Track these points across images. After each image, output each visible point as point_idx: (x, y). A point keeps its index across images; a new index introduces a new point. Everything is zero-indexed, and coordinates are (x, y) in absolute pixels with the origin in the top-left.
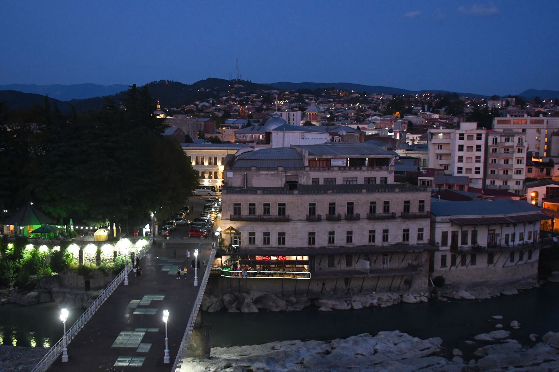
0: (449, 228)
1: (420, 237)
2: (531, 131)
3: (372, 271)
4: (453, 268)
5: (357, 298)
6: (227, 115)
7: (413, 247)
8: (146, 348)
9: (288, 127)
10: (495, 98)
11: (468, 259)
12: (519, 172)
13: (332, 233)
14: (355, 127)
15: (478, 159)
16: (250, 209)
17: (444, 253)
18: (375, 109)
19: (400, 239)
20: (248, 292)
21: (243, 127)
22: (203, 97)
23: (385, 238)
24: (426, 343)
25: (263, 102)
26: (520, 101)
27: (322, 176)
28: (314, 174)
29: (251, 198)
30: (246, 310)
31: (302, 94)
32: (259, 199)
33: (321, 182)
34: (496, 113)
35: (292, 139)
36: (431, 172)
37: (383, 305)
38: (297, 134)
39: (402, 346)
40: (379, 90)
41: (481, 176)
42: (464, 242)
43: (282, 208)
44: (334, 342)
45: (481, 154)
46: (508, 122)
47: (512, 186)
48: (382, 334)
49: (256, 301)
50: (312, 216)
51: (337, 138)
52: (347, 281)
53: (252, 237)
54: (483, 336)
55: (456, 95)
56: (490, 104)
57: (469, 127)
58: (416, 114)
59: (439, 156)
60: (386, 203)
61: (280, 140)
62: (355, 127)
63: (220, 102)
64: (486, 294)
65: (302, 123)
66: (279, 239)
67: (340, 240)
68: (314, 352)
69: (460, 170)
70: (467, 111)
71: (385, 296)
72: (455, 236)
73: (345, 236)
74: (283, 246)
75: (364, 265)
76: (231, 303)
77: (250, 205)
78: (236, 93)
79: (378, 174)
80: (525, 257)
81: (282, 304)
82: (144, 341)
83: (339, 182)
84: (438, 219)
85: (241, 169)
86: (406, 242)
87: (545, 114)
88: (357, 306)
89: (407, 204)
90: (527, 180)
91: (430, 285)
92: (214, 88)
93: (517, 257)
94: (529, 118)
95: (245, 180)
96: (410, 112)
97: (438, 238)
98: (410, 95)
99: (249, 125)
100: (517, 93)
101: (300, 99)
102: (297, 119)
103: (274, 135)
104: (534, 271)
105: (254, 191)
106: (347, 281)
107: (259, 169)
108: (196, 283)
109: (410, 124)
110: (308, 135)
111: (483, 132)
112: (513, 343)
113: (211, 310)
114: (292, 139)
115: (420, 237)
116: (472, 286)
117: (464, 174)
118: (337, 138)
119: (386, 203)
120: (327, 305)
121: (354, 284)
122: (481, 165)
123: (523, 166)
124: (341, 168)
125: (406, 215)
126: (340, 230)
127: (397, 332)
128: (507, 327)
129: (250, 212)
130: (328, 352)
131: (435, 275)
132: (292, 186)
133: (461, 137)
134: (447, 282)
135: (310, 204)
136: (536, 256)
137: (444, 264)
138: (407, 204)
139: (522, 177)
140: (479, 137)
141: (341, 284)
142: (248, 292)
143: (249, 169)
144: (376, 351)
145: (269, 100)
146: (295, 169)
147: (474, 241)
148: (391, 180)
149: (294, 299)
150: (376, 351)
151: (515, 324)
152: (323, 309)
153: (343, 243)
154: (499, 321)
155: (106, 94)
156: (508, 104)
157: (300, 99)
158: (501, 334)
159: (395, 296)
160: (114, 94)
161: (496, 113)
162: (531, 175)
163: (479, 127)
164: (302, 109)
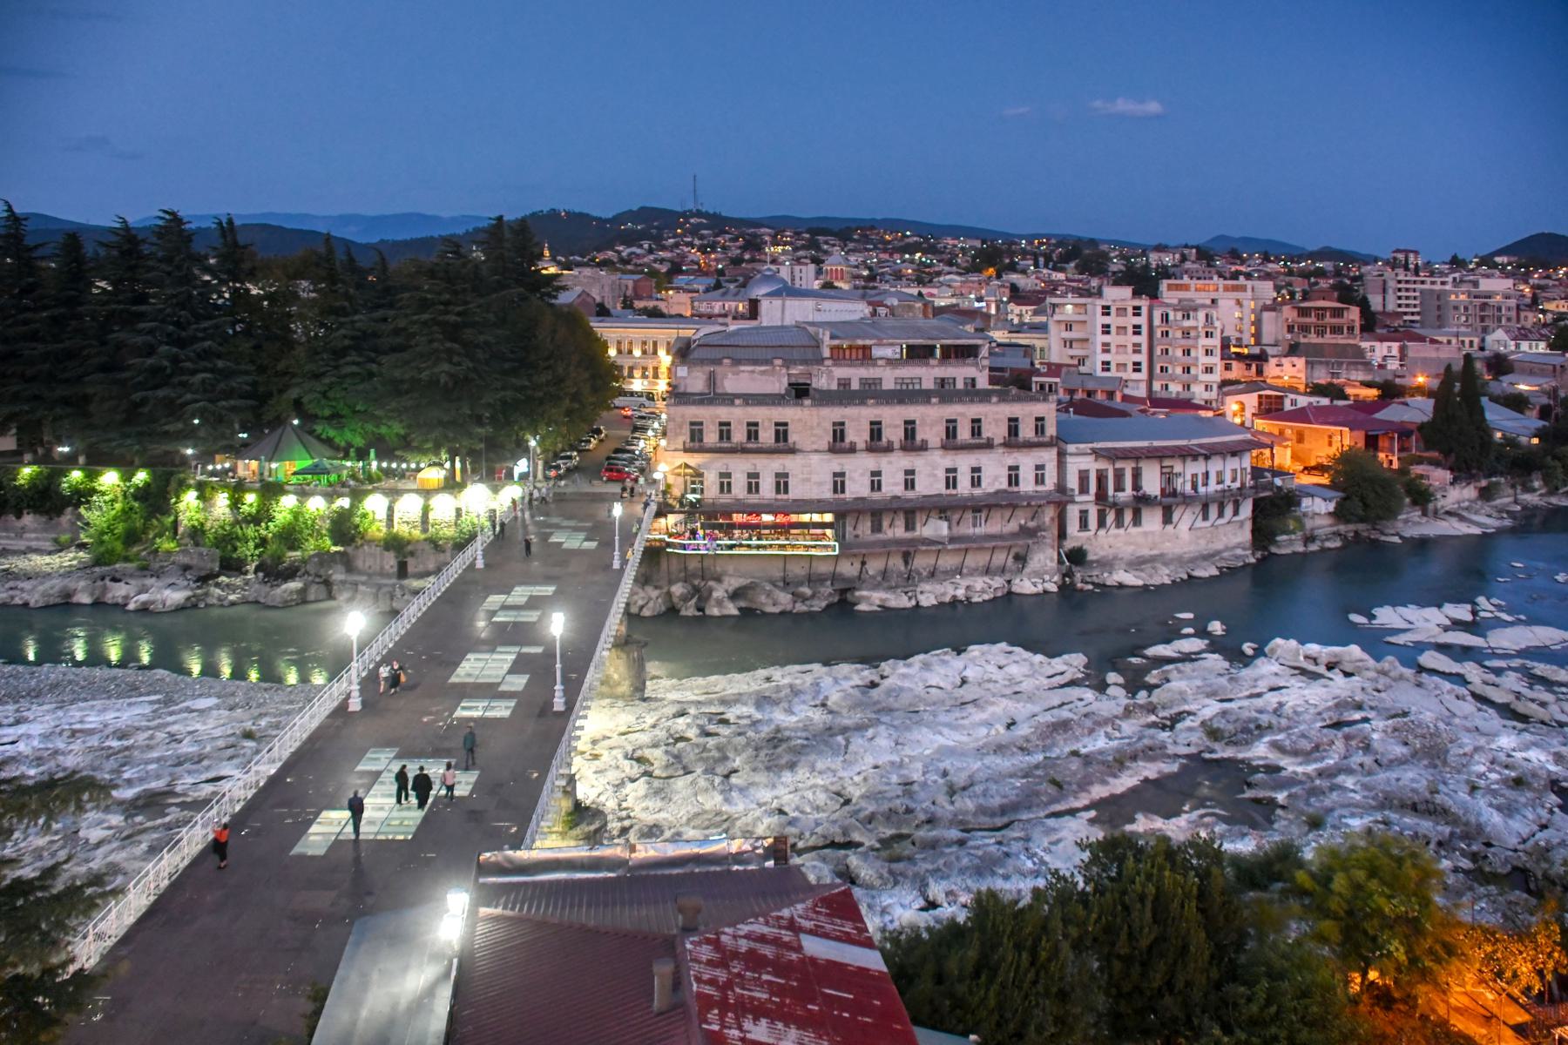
0: (1092, 465)
1: (1040, 480)
2: (1227, 303)
3: (952, 540)
5: (926, 587)
6: (676, 269)
8: (519, 682)
9: (789, 291)
10: (1160, 248)
14: (915, 291)
15: (1137, 349)
17: (1084, 507)
20: (719, 580)
21: (707, 290)
22: (631, 239)
24: (1058, 664)
25: (744, 248)
26: (1205, 255)
27: (856, 375)
28: (841, 372)
29: (723, 413)
30: (715, 612)
31: (815, 237)
32: (738, 415)
34: (1165, 273)
35: (798, 311)
38: (809, 304)
39: (1014, 670)
41: (1143, 375)
42: (1119, 487)
44: (886, 667)
45: (1143, 339)
46: (1186, 288)
47: (1199, 393)
48: (975, 650)
49: (735, 595)
51: (882, 311)
52: (907, 557)
55: (1093, 243)
56: (1154, 258)
59: (1069, 343)
61: (774, 313)
63: (664, 248)
65: (816, 285)
66: (778, 484)
67: (893, 486)
68: (846, 685)
70: (1114, 268)
71: (979, 583)
72: (1101, 478)
73: (901, 477)
75: (935, 528)
78: (694, 231)
79: (960, 373)
80: (1229, 510)
81: (784, 599)
83: (889, 385)
85: (702, 362)
86: (1015, 489)
87: (1248, 276)
88: (927, 600)
89: (1013, 425)
90: (1224, 383)
91: (1060, 562)
94: (1221, 282)
95: (712, 380)
96: (1012, 268)
97: (1073, 482)
99: (718, 286)
100: (1201, 239)
102: (807, 276)
103: (765, 306)
104: (1245, 535)
105: (729, 399)
106: (907, 557)
107: (737, 362)
108: (559, 704)
109: (1014, 288)
110: (826, 305)
111: (1144, 303)
112: (1215, 661)
113: (646, 613)
114: (798, 311)
115: (1040, 480)
116: (1137, 564)
117: (1113, 373)
118: (882, 311)
119: (976, 422)
120: (870, 600)
121: (921, 562)
122: (1143, 358)
124: (890, 362)
126: (893, 468)
127: (1003, 645)
128: (1202, 633)
129: (721, 438)
131: (1069, 544)
132: (800, 392)
133: (1106, 311)
134: (1091, 557)
136: (1246, 510)
138: (1013, 425)
139: (1216, 378)
140: (1137, 311)
141: (897, 563)
142: (719, 580)
143: (718, 362)
144: (964, 681)
145: (754, 245)
146: (805, 362)
147: (1136, 486)
148: (983, 383)
149: (806, 591)
150: (964, 681)
152: (862, 607)
153: (899, 490)
154: (1187, 623)
156: (1184, 259)
157: (813, 244)
159: (998, 582)
162: (1231, 375)
163: (1136, 294)
164: (817, 261)
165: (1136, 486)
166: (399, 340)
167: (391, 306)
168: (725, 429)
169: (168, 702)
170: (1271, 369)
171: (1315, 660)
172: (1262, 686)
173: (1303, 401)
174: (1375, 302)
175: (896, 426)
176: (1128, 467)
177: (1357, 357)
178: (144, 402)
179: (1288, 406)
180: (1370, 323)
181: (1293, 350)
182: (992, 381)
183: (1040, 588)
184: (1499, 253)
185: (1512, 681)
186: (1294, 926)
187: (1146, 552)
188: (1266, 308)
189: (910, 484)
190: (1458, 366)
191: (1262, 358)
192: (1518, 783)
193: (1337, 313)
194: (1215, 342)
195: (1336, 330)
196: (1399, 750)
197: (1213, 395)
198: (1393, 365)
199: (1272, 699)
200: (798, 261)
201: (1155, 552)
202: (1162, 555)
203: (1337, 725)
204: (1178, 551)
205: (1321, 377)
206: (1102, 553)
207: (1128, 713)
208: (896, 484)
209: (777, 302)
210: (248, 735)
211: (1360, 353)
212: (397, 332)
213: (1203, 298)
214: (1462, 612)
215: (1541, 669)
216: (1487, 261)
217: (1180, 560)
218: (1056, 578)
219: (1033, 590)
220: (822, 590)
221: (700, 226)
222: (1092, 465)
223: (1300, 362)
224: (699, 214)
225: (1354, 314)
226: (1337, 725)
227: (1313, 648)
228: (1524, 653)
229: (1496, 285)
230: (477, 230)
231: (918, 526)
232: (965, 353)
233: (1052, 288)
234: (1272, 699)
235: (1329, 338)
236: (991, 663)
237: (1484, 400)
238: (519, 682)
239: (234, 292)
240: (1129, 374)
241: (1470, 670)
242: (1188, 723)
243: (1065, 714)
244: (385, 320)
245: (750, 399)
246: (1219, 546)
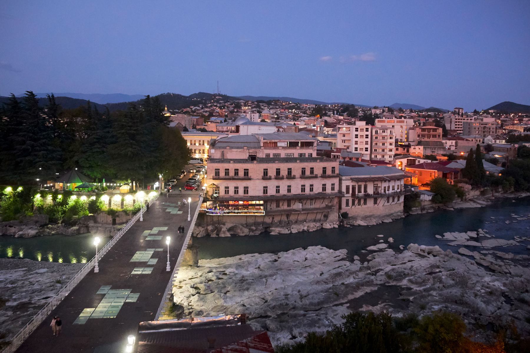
0: (350, 184)
1: (333, 189)
2: (397, 126)
3: (303, 210)
7: (329, 195)
8: (154, 261)
9: (250, 123)
10: (376, 108)
11: (362, 201)
12: (391, 150)
13: (278, 187)
15: (367, 143)
17: (347, 198)
18: (304, 113)
19: (320, 190)
20: (224, 224)
22: (196, 104)
24: (338, 253)
25: (234, 108)
27: (272, 152)
28: (267, 151)
29: (226, 166)
30: (223, 236)
31: (259, 104)
32: (232, 167)
33: (271, 156)
34: (377, 116)
35: (252, 130)
36: (339, 150)
37: (310, 231)
39: (323, 255)
40: (307, 102)
41: (369, 152)
42: (360, 191)
45: (369, 140)
46: (384, 121)
47: (387, 159)
48: (310, 248)
49: (229, 230)
51: (281, 130)
52: (288, 216)
55: (353, 106)
57: (361, 124)
58: (329, 116)
59: (344, 141)
61: (244, 130)
62: (292, 123)
63: (207, 107)
67: (283, 191)
68: (267, 261)
69: (356, 149)
70: (360, 115)
71: (312, 225)
72: (354, 188)
75: (298, 206)
76: (212, 231)
78: (218, 101)
79: (307, 151)
80: (396, 199)
81: (246, 231)
82: (152, 257)
83: (283, 156)
84: (344, 178)
86: (325, 192)
87: (405, 117)
88: (294, 231)
89: (324, 169)
90: (396, 155)
91: (339, 217)
92: (203, 99)
93: (391, 200)
95: (223, 154)
96: (325, 115)
97: (344, 190)
98: (325, 106)
101: (258, 106)
102: (256, 117)
103: (241, 128)
104: (402, 208)
105: (229, 161)
106: (288, 216)
107: (232, 148)
108: (168, 268)
109: (326, 122)
111: (369, 127)
112: (390, 251)
113: (199, 236)
114: (252, 130)
115: (333, 189)
116: (365, 218)
117: (358, 152)
118: (281, 130)
120: (275, 231)
121: (293, 218)
122: (368, 146)
123: (393, 147)
124: (283, 148)
125: (324, 175)
126: (284, 185)
128: (386, 242)
129: (226, 175)
130: (276, 261)
131: (342, 211)
132: (253, 158)
133: (357, 130)
134: (350, 216)
136: (402, 199)
137: (347, 205)
138: (324, 169)
139: (393, 153)
140: (367, 130)
141: (284, 218)
142: (224, 224)
143: (225, 148)
144: (306, 259)
145: (238, 106)
146: (255, 148)
147: (365, 191)
148: (314, 155)
149: (254, 228)
150: (306, 259)
151: (391, 240)
152: (272, 233)
154: (381, 238)
155: (130, 101)
156: (384, 111)
157: (258, 106)
158: (383, 246)
159: (318, 224)
160: (136, 100)
161: (377, 116)
162: (398, 152)
163: (367, 124)
164: (259, 112)
165: (365, 191)
166: (114, 139)
167: (111, 127)
168: (227, 171)
169: (29, 270)
170: (412, 150)
171: (424, 251)
172: (406, 260)
173: (422, 161)
174: (448, 126)
176: (363, 184)
177: (441, 146)
178: (21, 161)
179: (417, 163)
180: (446, 134)
181: (419, 143)
182: (318, 154)
183: (332, 226)
184: (490, 109)
185: (490, 258)
187: (368, 214)
188: (410, 129)
189: (289, 191)
190: (475, 149)
191: (409, 146)
192: (491, 293)
193: (435, 130)
194: (393, 140)
195: (434, 136)
196: (452, 282)
197: (392, 159)
198: (453, 148)
199: (409, 264)
200: (253, 112)
202: (373, 215)
203: (430, 274)
204: (379, 213)
205: (429, 153)
207: (361, 270)
208: (285, 191)
209: (246, 127)
210: (59, 282)
211: (442, 144)
212: (113, 136)
213: (390, 125)
214: (474, 234)
215: (499, 254)
216: (486, 112)
217: (379, 217)
221: (219, 99)
222: (350, 184)
223: (422, 148)
224: (219, 95)
225: (440, 131)
226: (430, 274)
227: (423, 247)
228: (494, 248)
229: (489, 120)
230: (142, 100)
231: (292, 205)
232: (308, 145)
233: (339, 122)
234: (409, 264)
235: (432, 139)
236: (315, 252)
237: (483, 160)
238: (154, 261)
239: (55, 122)
240: (364, 152)
241: (476, 254)
242: (381, 273)
243: (340, 270)
244: (109, 132)
245: (236, 161)
246: (392, 212)
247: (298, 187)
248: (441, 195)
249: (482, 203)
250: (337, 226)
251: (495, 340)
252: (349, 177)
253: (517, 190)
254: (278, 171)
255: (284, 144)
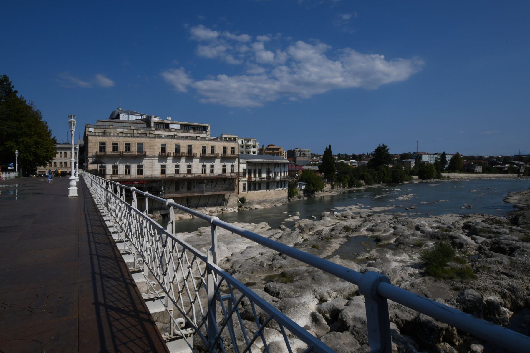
4: (249, 192)
16: (114, 147)
17: (244, 182)
19: (221, 171)
23: (212, 171)
43: (140, 147)
50: (163, 156)
53: (115, 169)
54: (401, 214)
60: (213, 148)
64: (268, 206)
66: (138, 170)
74: (141, 176)
77: (114, 144)
84: (241, 161)
86: (225, 174)
89: (225, 149)
91: (238, 202)
115: (232, 171)
116: (260, 203)
119: (213, 148)
124: (176, 130)
129: (114, 150)
131: (240, 196)
134: (247, 201)
135: (162, 145)
175: (185, 147)
183: (233, 211)
186: (456, 255)
187: (262, 199)
201: (264, 199)
202: (266, 200)
204: (270, 198)
206: (249, 199)
208: (185, 171)
217: (271, 202)
218: (237, 208)
219: (231, 211)
220: (157, 215)
231: (192, 188)
246: (280, 197)
247: (198, 168)
248: (313, 184)
249: (334, 193)
250: (237, 211)
251: (487, 248)
252: (245, 161)
253: (350, 186)
254: (177, 149)
255: (177, 127)
